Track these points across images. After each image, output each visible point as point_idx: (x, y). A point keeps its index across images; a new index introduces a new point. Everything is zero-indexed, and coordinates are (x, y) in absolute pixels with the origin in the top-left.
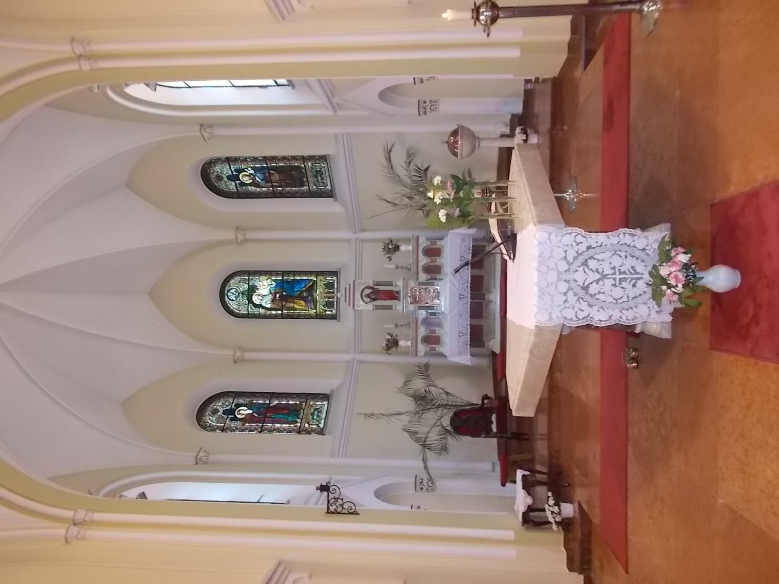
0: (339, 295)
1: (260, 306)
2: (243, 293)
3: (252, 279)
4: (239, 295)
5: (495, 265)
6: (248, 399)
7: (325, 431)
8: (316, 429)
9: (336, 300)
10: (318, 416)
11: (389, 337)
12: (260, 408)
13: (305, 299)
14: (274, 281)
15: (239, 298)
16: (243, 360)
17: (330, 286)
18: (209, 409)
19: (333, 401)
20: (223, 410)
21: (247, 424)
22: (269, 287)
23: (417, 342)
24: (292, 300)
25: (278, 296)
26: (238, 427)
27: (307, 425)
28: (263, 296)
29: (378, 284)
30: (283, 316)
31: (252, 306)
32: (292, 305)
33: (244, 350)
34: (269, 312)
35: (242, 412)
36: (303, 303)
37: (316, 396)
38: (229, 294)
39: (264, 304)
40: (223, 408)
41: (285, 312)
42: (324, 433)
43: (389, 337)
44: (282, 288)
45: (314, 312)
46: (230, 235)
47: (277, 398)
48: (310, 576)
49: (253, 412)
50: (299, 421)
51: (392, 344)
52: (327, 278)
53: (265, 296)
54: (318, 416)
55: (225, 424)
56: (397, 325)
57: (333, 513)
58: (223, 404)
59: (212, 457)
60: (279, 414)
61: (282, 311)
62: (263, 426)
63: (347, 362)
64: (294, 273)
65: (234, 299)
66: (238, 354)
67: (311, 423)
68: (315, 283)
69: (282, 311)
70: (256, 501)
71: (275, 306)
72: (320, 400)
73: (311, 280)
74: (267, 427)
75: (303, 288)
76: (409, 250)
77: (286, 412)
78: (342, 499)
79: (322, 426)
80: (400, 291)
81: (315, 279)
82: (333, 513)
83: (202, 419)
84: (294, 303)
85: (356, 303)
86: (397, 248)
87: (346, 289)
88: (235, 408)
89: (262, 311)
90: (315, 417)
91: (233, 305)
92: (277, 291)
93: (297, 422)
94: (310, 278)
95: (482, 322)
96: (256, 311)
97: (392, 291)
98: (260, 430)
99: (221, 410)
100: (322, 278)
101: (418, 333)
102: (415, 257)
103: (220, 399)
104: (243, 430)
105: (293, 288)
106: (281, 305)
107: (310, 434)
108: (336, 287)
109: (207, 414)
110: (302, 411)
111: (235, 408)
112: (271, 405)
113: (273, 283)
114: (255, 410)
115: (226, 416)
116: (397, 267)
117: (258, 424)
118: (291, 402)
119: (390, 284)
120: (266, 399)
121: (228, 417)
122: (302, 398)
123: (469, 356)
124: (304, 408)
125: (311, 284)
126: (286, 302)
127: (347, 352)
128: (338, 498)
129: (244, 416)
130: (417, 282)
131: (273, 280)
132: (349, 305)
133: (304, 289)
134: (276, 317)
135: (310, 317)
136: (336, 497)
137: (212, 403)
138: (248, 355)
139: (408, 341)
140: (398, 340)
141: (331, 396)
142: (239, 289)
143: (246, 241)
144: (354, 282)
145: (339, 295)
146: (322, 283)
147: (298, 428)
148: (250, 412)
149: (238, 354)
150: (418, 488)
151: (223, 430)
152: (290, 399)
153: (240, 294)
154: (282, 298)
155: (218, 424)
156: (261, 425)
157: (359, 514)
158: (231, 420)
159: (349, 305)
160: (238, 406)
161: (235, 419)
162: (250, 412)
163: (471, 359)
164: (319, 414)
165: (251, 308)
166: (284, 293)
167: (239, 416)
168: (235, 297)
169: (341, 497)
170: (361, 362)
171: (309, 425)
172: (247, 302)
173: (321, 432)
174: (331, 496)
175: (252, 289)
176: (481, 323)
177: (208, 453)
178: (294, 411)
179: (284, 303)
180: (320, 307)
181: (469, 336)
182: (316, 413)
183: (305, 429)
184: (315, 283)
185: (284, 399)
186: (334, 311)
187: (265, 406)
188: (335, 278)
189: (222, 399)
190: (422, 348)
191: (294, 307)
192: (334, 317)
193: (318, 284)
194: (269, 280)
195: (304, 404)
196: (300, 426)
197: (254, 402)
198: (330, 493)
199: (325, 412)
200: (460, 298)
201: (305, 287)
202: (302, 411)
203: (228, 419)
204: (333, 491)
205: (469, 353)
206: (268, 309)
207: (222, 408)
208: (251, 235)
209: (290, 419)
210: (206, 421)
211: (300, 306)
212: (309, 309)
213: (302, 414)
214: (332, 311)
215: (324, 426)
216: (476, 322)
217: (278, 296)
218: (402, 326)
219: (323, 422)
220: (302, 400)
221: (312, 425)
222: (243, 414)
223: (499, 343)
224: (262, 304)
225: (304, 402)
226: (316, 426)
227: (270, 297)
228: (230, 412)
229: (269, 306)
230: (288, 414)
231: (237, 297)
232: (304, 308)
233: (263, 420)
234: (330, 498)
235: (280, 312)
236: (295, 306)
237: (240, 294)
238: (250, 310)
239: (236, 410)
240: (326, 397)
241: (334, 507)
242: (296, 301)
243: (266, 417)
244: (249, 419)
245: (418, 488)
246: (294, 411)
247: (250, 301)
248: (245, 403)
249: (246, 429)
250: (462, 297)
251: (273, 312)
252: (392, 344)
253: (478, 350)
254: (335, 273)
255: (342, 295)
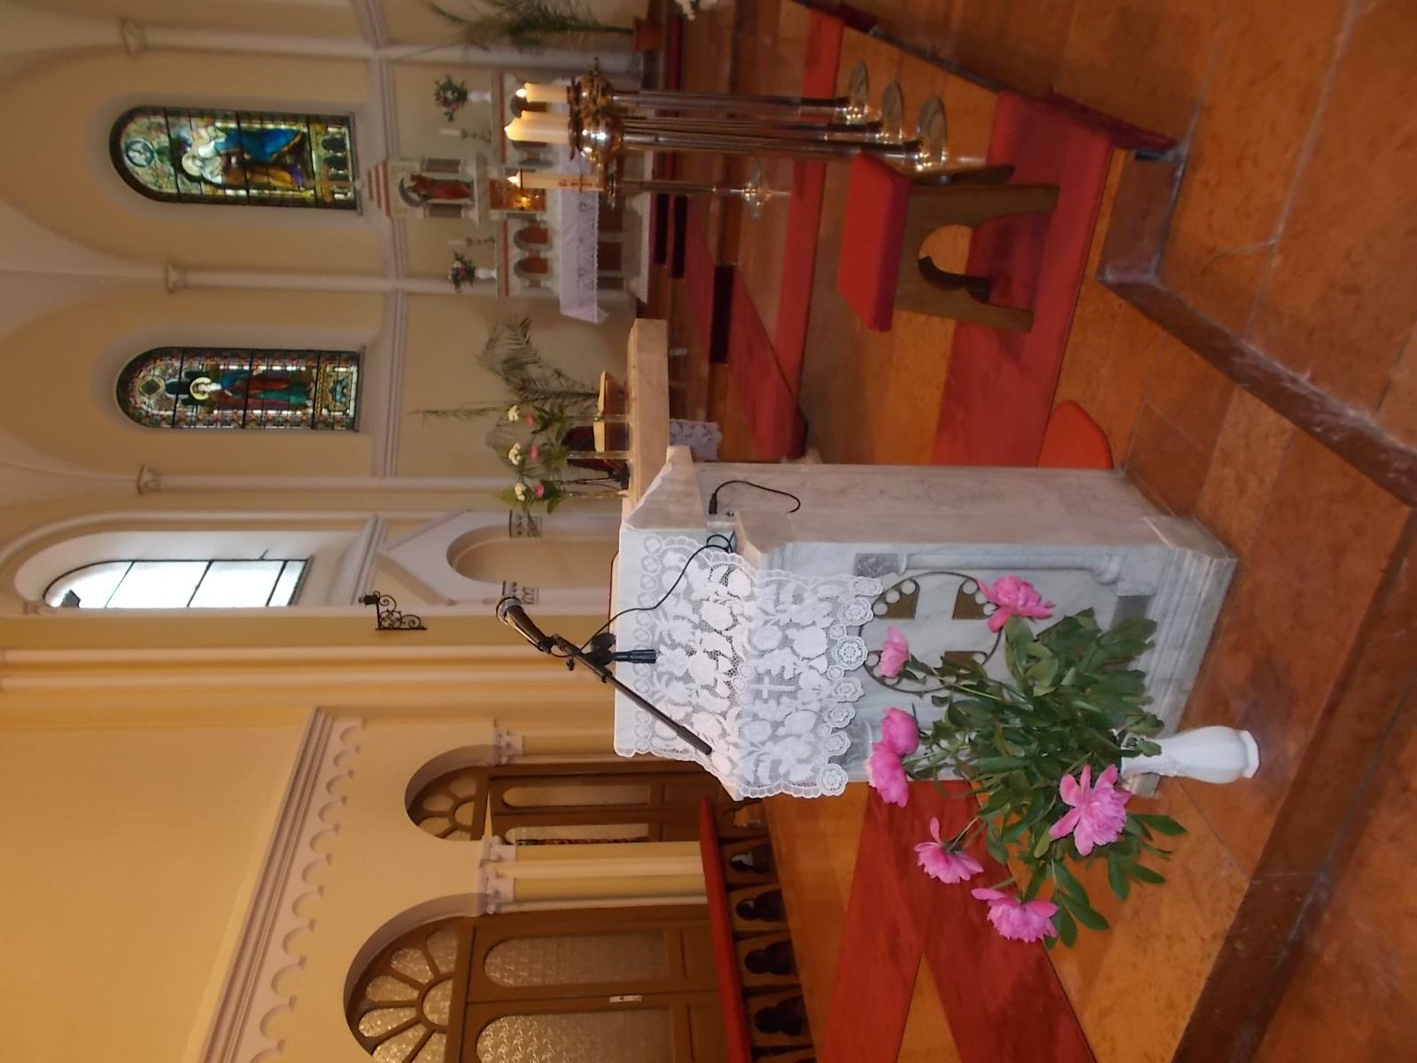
0: (358, 184)
1: (200, 180)
2: (160, 152)
3: (174, 125)
4: (153, 157)
5: (640, 230)
6: (209, 362)
7: (359, 426)
8: (342, 419)
9: (351, 173)
10: (343, 395)
11: (457, 265)
12: (234, 381)
13: (289, 169)
14: (222, 130)
15: (153, 162)
16: (186, 287)
17: (334, 144)
18: (139, 383)
19: (367, 365)
20: (167, 386)
21: (216, 412)
22: (213, 143)
23: (507, 276)
24: (264, 170)
25: (233, 160)
26: (200, 417)
27: (325, 412)
28: (204, 160)
29: (434, 164)
30: (249, 201)
31: (185, 179)
32: (265, 180)
33: (184, 268)
34: (220, 192)
35: (202, 388)
36: (287, 177)
37: (335, 357)
38: (131, 154)
39: (208, 177)
40: (165, 380)
41: (253, 192)
42: (356, 428)
43: (457, 265)
44: (241, 145)
45: (312, 195)
46: (109, 35)
47: (263, 358)
48: (365, 722)
49: (223, 388)
50: (310, 403)
51: (465, 274)
52: (330, 129)
53: (207, 159)
54: (343, 395)
55: (175, 411)
56: (470, 241)
57: (386, 629)
58: (164, 373)
59: (167, 481)
60: (272, 390)
61: (248, 192)
62: (245, 415)
63: (384, 293)
64: (262, 117)
65: (145, 163)
66: (174, 276)
67: (331, 407)
68: (305, 138)
69: (248, 192)
70: (257, 558)
71: (231, 181)
72: (343, 364)
73: (297, 132)
74: (253, 417)
75: (284, 146)
76: (486, 103)
77: (284, 386)
78: (400, 613)
79: (351, 412)
80: (472, 182)
81: (305, 130)
82: (386, 629)
83: (130, 402)
84: (268, 175)
85: (392, 204)
86: (462, 96)
87: (369, 174)
88: (188, 380)
89: (206, 189)
90: (338, 397)
91: (144, 175)
92: (230, 150)
93: (306, 407)
94: (294, 128)
95: (620, 238)
96: (195, 189)
97: (456, 181)
98: (241, 423)
99: (162, 384)
100: (318, 128)
101: (510, 257)
102: (498, 115)
103: (155, 363)
104: (210, 423)
105: (263, 145)
106: (243, 179)
107: (333, 429)
108: (348, 146)
109: (137, 394)
110: (312, 385)
111: (188, 380)
112: (255, 373)
113: (220, 134)
114: (226, 384)
115: (173, 397)
116: (465, 135)
117: (235, 411)
118: (290, 368)
119: (452, 165)
120: (243, 362)
121: (177, 399)
122: (310, 360)
123: (596, 308)
124: (315, 379)
125: (297, 139)
126: (253, 172)
127: (383, 275)
128: (393, 611)
129: (206, 397)
130: (504, 167)
131: (218, 128)
132: (380, 206)
133: (286, 148)
134: (236, 201)
135: (301, 203)
136: (391, 609)
137: (141, 371)
138: (195, 278)
139: (492, 269)
140: (474, 268)
141: (351, 120)
142: (151, 144)
143: (144, 48)
144: (385, 165)
145: (358, 184)
146: (321, 139)
147: (310, 416)
148: (215, 387)
149: (174, 276)
150: (514, 532)
151: (174, 423)
152: (286, 361)
153: (156, 155)
154: (243, 165)
155: (162, 413)
156: (241, 412)
157: (424, 629)
158: (185, 403)
159: (380, 206)
160: (193, 375)
161: (192, 402)
162: (215, 387)
163: (598, 312)
164: (345, 391)
165: (183, 183)
166: (246, 156)
167: (198, 397)
168: (146, 160)
169: (397, 609)
170: (410, 294)
171: (329, 411)
172: (172, 170)
173: (352, 425)
174: (382, 609)
175: (177, 150)
176: (620, 276)
177: (156, 473)
178: (296, 387)
179: (248, 176)
180: (317, 140)
181: (597, 213)
182: (339, 388)
183: (322, 419)
184: (305, 138)
185: (276, 362)
186: (349, 194)
187: (242, 376)
188: (344, 130)
189: (158, 362)
190: (516, 283)
191: (269, 183)
192: (349, 206)
193: (313, 140)
194: (211, 129)
195: (315, 371)
196: (313, 414)
197: (222, 367)
198: (380, 607)
199: (354, 386)
200: (581, 210)
201: (287, 144)
202: (312, 385)
203: (179, 402)
204: (384, 601)
205: (596, 304)
206: (217, 186)
207: (162, 381)
208: (156, 37)
209: (293, 399)
210: (138, 406)
211: (281, 183)
212: (301, 188)
213: (314, 390)
214: (346, 194)
215: (355, 414)
216: (608, 238)
217: (233, 160)
218: (479, 242)
219: (352, 405)
220: (310, 363)
221: (334, 411)
222: (204, 393)
223: (646, 285)
224: (204, 175)
225: (313, 367)
226: (341, 413)
227: (219, 161)
228: (181, 388)
229: (219, 180)
230: (289, 391)
231: (149, 161)
232: (290, 186)
233: (243, 403)
234: (380, 611)
235: (242, 193)
236: (272, 181)
237: (156, 155)
238: (180, 186)
239: (190, 384)
240: (354, 358)
241: (389, 622)
242: (272, 171)
243: (247, 396)
244: (216, 401)
245: (514, 532)
246: (296, 387)
247: (179, 168)
248: (204, 370)
249: (216, 421)
250: (583, 207)
251: (230, 192)
252: (465, 274)
253: (612, 295)
254: (343, 121)
255: (363, 186)
